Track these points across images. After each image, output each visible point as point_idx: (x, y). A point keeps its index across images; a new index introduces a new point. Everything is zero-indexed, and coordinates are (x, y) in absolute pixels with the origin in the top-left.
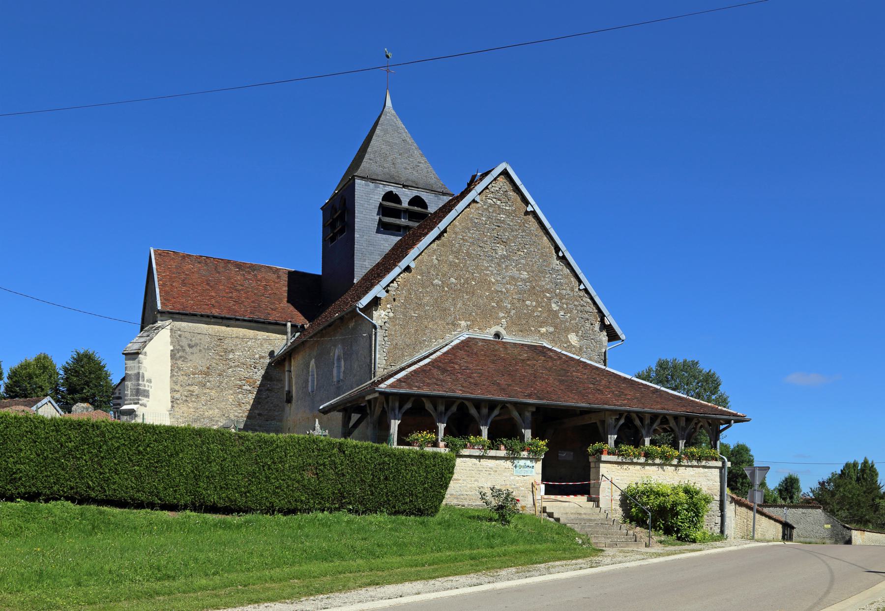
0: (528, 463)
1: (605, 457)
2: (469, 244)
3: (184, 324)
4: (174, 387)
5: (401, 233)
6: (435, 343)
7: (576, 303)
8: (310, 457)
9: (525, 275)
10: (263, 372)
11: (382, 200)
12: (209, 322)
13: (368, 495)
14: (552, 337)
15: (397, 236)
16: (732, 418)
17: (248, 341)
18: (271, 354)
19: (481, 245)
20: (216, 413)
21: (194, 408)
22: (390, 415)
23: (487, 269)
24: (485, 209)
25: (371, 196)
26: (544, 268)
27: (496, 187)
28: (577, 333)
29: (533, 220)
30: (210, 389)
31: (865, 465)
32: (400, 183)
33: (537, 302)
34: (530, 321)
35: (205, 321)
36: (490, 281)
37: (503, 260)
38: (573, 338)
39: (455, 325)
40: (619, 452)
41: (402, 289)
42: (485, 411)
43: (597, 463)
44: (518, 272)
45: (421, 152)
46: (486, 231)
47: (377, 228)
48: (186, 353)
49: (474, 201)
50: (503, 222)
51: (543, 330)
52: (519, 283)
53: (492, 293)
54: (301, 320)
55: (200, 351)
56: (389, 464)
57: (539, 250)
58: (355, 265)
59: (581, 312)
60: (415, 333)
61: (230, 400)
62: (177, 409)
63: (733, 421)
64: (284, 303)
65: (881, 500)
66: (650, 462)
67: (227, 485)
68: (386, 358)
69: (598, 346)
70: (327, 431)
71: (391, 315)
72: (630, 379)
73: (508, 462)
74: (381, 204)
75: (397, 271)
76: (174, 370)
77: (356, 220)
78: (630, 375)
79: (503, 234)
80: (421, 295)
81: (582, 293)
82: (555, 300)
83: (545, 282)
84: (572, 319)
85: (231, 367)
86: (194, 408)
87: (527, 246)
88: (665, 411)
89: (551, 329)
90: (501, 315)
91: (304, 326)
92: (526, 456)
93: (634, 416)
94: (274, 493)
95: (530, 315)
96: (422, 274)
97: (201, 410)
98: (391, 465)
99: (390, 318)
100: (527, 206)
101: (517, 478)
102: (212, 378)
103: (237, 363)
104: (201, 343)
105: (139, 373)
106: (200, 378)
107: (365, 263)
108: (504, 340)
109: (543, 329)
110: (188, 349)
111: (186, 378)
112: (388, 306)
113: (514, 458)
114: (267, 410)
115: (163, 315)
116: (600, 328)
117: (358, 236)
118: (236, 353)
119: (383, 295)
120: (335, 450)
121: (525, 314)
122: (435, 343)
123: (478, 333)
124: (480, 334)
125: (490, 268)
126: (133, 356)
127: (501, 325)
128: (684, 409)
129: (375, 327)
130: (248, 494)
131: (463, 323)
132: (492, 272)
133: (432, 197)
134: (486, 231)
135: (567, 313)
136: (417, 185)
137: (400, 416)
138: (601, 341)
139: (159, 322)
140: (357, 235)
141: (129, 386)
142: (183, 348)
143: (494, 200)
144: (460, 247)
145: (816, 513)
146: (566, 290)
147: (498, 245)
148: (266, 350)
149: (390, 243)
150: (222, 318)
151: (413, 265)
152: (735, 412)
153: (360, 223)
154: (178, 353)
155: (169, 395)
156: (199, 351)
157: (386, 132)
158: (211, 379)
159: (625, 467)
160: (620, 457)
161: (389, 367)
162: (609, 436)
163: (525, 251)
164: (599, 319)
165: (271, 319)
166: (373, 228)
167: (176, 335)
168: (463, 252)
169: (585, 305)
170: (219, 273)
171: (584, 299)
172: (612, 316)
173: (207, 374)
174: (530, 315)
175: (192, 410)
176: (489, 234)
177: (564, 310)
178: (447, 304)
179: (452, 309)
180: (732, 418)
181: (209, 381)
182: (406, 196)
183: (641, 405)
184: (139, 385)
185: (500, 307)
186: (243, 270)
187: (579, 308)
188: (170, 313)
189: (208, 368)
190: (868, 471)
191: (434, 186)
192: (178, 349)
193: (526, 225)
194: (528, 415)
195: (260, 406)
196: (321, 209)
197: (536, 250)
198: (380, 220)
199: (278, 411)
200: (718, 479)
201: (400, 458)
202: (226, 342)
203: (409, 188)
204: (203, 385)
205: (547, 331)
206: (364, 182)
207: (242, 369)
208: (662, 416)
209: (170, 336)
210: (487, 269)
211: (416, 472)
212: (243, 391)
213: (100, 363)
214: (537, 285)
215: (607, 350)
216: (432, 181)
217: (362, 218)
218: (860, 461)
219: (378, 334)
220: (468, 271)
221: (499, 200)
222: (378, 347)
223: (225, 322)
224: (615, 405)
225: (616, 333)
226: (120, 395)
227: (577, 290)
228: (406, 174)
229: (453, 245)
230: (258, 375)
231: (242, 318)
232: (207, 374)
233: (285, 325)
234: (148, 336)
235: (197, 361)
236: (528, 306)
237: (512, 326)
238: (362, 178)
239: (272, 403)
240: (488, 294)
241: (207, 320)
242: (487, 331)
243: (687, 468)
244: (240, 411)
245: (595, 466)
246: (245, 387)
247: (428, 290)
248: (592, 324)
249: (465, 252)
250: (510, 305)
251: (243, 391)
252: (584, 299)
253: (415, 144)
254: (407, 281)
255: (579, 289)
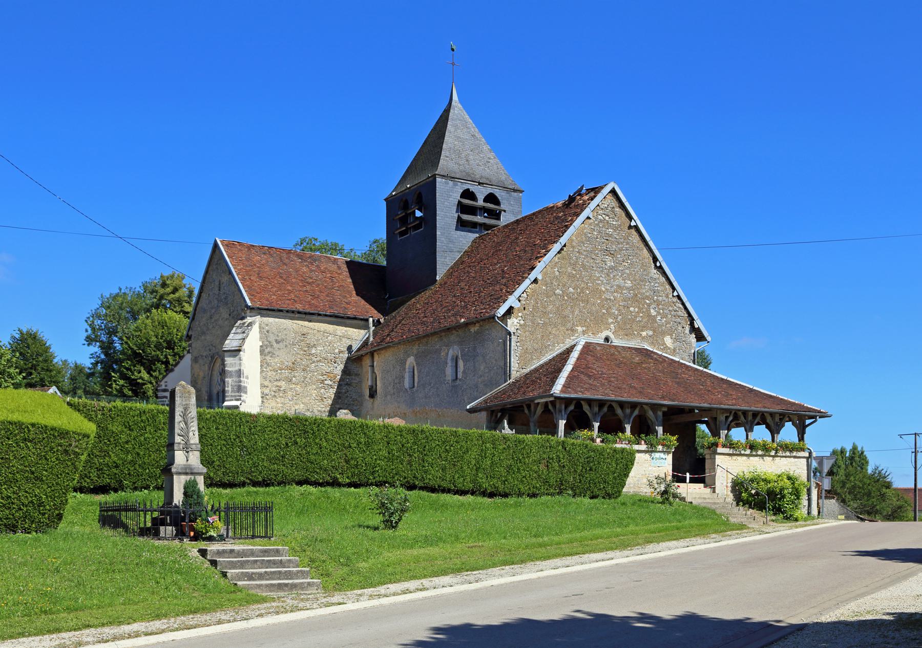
0: (662, 455)
1: (720, 450)
2: (584, 257)
3: (271, 320)
4: (263, 382)
5: (478, 230)
6: (558, 348)
7: (671, 308)
8: (544, 453)
9: (629, 284)
10: (342, 366)
11: (461, 197)
12: (294, 317)
13: (577, 482)
14: (652, 340)
15: (474, 233)
16: (817, 414)
17: (329, 336)
18: (350, 348)
19: (593, 257)
20: (301, 408)
21: (282, 403)
22: (557, 415)
23: (598, 279)
24: (596, 224)
25: (451, 194)
26: (644, 276)
27: (606, 203)
28: (671, 335)
29: (635, 233)
30: (296, 384)
31: (854, 451)
32: (476, 181)
33: (639, 308)
34: (633, 326)
35: (290, 317)
36: (601, 290)
37: (611, 271)
38: (668, 341)
39: (573, 330)
40: (730, 444)
41: (531, 299)
42: (628, 411)
43: (712, 455)
44: (623, 282)
45: (489, 148)
46: (597, 244)
47: (456, 225)
48: (274, 349)
49: (588, 218)
50: (611, 236)
51: (644, 334)
52: (625, 292)
53: (602, 300)
54: (377, 315)
55: (286, 346)
56: (594, 458)
57: (640, 260)
58: (437, 262)
59: (674, 316)
60: (542, 338)
61: (314, 395)
62: (266, 405)
63: (818, 417)
64: (355, 298)
65: (888, 490)
66: (754, 453)
67: (494, 475)
68: (518, 362)
69: (688, 347)
70: (514, 430)
71: (522, 322)
72: (726, 380)
73: (647, 454)
74: (459, 202)
75: (527, 282)
76: (263, 366)
77: (437, 217)
78: (725, 376)
79: (611, 247)
80: (546, 304)
81: (675, 299)
82: (653, 306)
83: (645, 290)
84: (667, 323)
85: (314, 362)
86: (282, 403)
87: (630, 257)
88: (763, 409)
89: (651, 333)
90: (610, 320)
91: (380, 321)
92: (661, 450)
93: (740, 413)
94: (522, 481)
95: (634, 320)
96: (546, 285)
97: (288, 405)
98: (595, 458)
99: (521, 325)
100: (631, 221)
101: (654, 468)
102: (297, 373)
103: (319, 358)
104: (286, 339)
105: (240, 370)
106: (286, 373)
107: (446, 260)
108: (612, 344)
109: (644, 333)
110: (275, 345)
111: (275, 374)
112: (520, 314)
113: (652, 452)
114: (346, 404)
115: (253, 311)
116: (690, 331)
117: (439, 233)
118: (319, 348)
119: (517, 305)
120: (560, 447)
121: (629, 319)
122: (558, 348)
123: (591, 338)
124: (594, 338)
125: (601, 278)
126: (234, 353)
127: (610, 330)
128: (779, 407)
129: (510, 334)
130: (506, 482)
131: (580, 329)
132: (602, 281)
133: (504, 194)
134: (597, 244)
135: (663, 318)
136: (490, 182)
137: (566, 416)
138: (690, 343)
139: (248, 318)
140: (438, 233)
141: (230, 382)
142: (271, 344)
143: (604, 216)
144: (577, 259)
145: (829, 503)
146: (662, 296)
147: (607, 257)
148: (345, 345)
149: (468, 240)
150: (305, 313)
151: (540, 277)
152: (819, 409)
153: (441, 221)
154: (267, 348)
155: (260, 391)
156: (286, 347)
157: (456, 126)
158: (296, 374)
159: (734, 458)
160: (732, 450)
161: (521, 370)
162: (721, 431)
163: (629, 261)
164: (689, 323)
165: (349, 314)
166: (452, 225)
167: (264, 330)
168: (579, 264)
169: (678, 310)
170: (285, 264)
171: (677, 305)
172: (700, 320)
173: (292, 369)
174: (634, 320)
175: (280, 405)
176: (599, 247)
177: (661, 314)
178: (567, 312)
179: (571, 316)
180: (817, 414)
181: (294, 377)
182: (481, 193)
183: (747, 405)
184: (240, 381)
185: (609, 313)
186: (305, 261)
187: (672, 313)
188: (259, 309)
189: (293, 364)
190: (857, 459)
191: (506, 183)
192: (267, 345)
193: (630, 238)
194: (660, 414)
195: (340, 401)
196: (385, 200)
197: (638, 261)
198: (459, 217)
199: (356, 406)
200: (805, 468)
201: (601, 452)
202: (309, 337)
203: (484, 185)
204: (289, 380)
205: (647, 334)
206: (444, 180)
207: (323, 364)
208: (761, 413)
209: (259, 332)
210: (598, 279)
211: (610, 464)
212: (325, 386)
213: (46, 344)
214: (639, 293)
215: (696, 351)
216: (503, 178)
217: (442, 216)
218: (848, 448)
219: (512, 340)
220: (583, 282)
221: (607, 216)
222: (512, 352)
223: (308, 317)
224: (728, 405)
225: (703, 335)
226: (166, 388)
227: (671, 296)
228: (480, 171)
229: (571, 258)
230: (338, 369)
231: (324, 313)
232: (292, 369)
233: (367, 320)
234: (244, 332)
235: (283, 357)
236: (631, 312)
237: (619, 330)
238: (443, 176)
239: (351, 398)
240: (599, 302)
241: (292, 315)
242: (599, 335)
243: (782, 459)
244: (323, 406)
245: (711, 457)
246: (326, 382)
247: (551, 299)
248: (683, 328)
249: (581, 264)
250: (617, 312)
251: (325, 386)
252: (677, 305)
253: (483, 139)
254: (534, 291)
255: (673, 296)
